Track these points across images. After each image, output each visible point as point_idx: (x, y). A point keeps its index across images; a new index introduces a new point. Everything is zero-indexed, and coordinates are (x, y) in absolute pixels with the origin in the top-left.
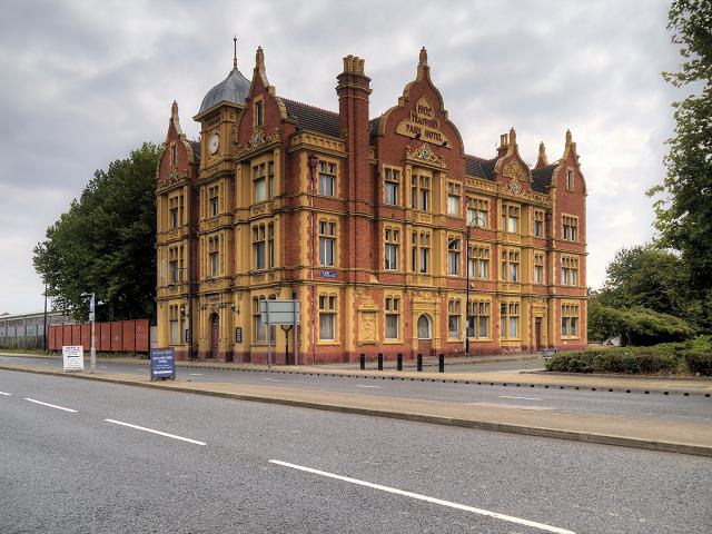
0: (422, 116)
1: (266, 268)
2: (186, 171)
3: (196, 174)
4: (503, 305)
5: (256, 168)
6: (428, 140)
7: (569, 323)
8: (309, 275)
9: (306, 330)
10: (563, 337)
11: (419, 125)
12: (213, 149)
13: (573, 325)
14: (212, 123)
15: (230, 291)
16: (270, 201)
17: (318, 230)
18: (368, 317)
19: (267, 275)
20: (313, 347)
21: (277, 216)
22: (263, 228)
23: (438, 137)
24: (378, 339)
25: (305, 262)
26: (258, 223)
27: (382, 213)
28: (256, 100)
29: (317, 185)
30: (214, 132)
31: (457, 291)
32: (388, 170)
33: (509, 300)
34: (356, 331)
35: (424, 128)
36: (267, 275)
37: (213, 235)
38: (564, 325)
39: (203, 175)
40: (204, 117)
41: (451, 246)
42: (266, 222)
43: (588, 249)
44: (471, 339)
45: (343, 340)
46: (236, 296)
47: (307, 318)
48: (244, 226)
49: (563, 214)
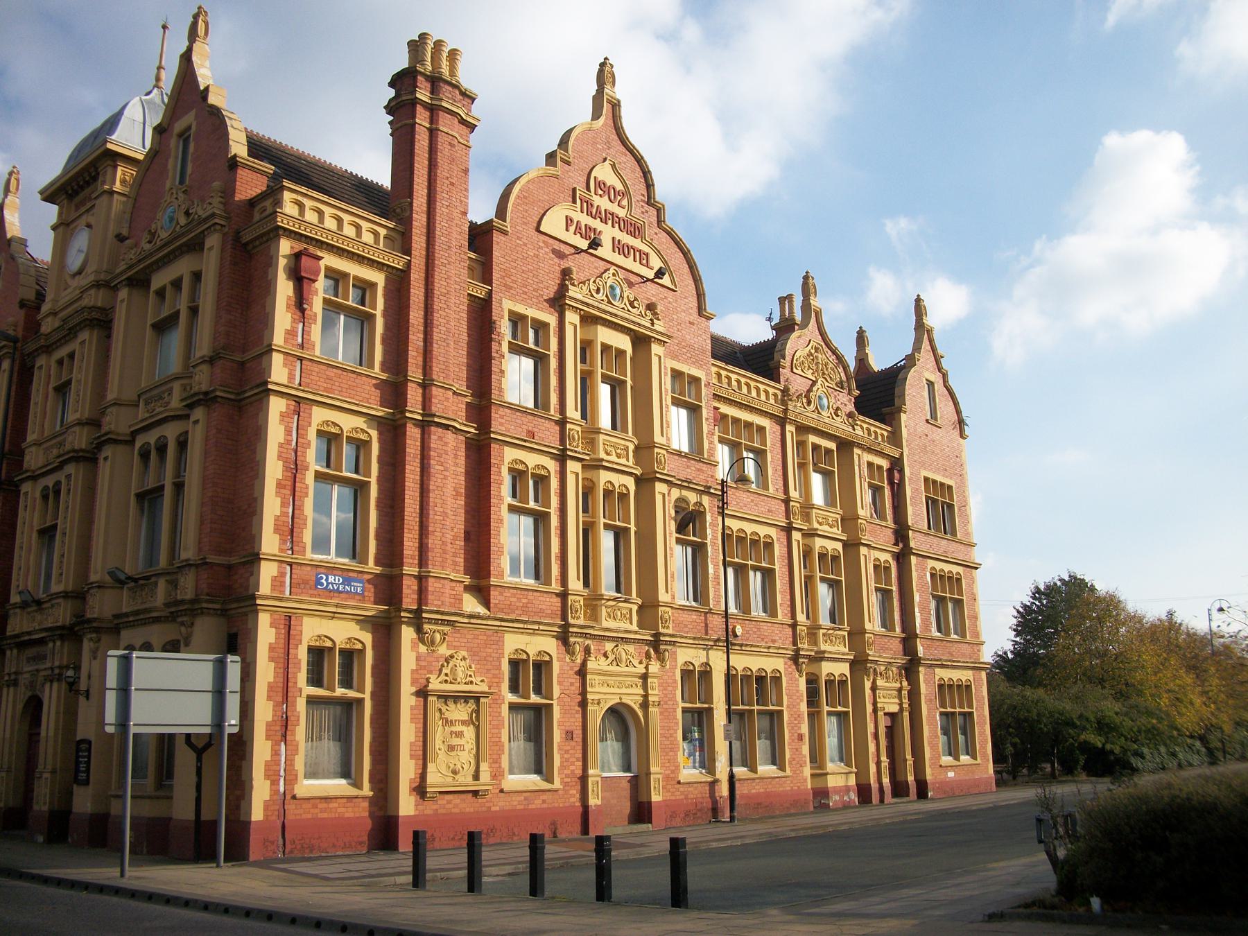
0: (603, 203)
4: (812, 681)
5: (161, 293)
6: (618, 259)
8: (277, 582)
9: (261, 750)
11: (596, 224)
16: (186, 375)
17: (302, 677)
18: (459, 712)
19: (162, 583)
20: (283, 800)
21: (199, 413)
22: (162, 449)
23: (643, 258)
25: (270, 542)
26: (151, 438)
27: (500, 423)
28: (179, 126)
30: (83, 221)
33: (827, 668)
35: (608, 233)
36: (162, 583)
39: (48, 326)
44: (740, 771)
48: (120, 449)
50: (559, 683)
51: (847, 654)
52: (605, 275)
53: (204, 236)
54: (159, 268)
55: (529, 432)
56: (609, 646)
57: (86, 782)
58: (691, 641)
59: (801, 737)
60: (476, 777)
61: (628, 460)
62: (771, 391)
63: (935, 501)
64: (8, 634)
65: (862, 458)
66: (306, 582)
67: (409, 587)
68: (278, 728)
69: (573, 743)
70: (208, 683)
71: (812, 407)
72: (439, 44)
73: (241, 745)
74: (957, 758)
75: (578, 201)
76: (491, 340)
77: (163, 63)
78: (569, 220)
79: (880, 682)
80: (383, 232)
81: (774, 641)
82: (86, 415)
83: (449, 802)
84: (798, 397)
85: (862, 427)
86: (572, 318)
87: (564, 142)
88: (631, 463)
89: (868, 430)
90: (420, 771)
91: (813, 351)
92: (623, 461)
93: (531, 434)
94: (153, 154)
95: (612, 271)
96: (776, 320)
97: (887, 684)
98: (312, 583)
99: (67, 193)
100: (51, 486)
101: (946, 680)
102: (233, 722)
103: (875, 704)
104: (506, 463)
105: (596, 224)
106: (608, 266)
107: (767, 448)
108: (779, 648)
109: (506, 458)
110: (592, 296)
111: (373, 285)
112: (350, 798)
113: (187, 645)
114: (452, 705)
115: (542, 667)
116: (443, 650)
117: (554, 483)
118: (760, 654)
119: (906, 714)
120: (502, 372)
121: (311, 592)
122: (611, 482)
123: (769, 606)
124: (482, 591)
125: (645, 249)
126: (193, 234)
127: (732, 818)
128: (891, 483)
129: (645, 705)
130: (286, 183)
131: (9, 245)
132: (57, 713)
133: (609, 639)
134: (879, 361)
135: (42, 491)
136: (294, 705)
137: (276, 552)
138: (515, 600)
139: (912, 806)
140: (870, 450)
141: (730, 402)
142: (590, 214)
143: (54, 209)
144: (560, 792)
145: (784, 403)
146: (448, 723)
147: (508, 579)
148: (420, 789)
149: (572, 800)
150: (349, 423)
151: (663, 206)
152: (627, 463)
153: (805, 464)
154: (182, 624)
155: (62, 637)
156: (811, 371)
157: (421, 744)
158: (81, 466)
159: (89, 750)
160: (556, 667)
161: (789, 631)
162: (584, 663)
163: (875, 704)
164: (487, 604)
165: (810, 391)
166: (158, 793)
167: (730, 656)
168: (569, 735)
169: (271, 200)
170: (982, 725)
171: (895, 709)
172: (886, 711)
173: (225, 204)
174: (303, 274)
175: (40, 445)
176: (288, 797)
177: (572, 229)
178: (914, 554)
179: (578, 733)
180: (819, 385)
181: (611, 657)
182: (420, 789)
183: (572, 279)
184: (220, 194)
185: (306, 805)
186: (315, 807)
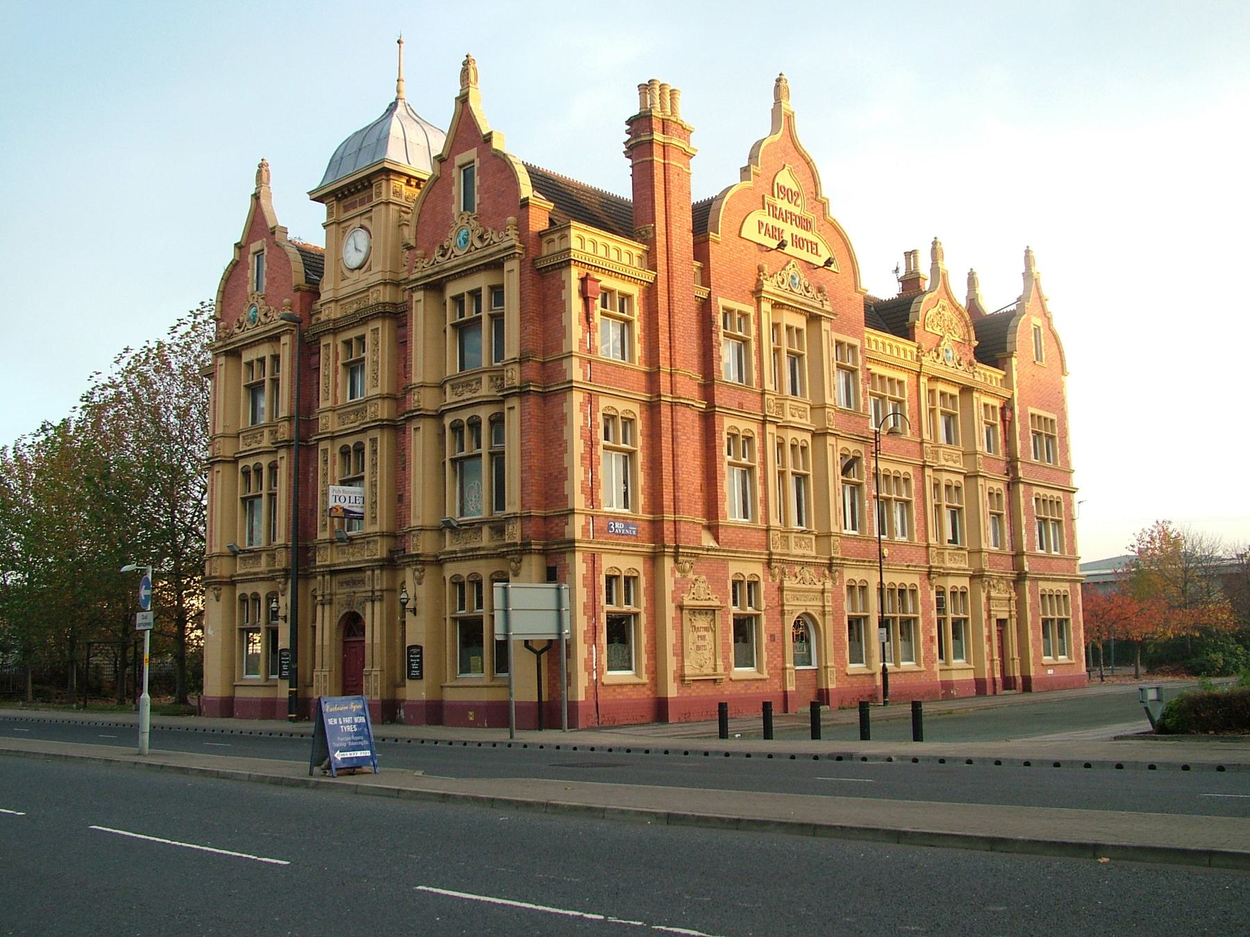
0: (783, 204)
1: (263, 544)
2: (289, 302)
3: (310, 312)
4: (940, 593)
7: (1053, 631)
8: (585, 530)
10: (1047, 659)
11: (779, 224)
12: (353, 258)
13: (956, 635)
14: (353, 206)
15: (392, 563)
18: (702, 622)
20: (596, 685)
22: (258, 470)
23: (813, 247)
24: (720, 670)
25: (579, 501)
26: (251, 463)
27: (720, 398)
29: (598, 337)
30: (357, 222)
31: (861, 562)
32: (728, 312)
33: (950, 583)
34: (681, 654)
37: (351, 442)
38: (1046, 635)
40: (333, 193)
41: (845, 471)
42: (265, 461)
43: (1076, 481)
45: (657, 672)
46: (409, 575)
47: (582, 623)
49: (1031, 410)
50: (765, 598)
51: (967, 570)
52: (788, 268)
53: (504, 260)
54: (455, 279)
55: (739, 403)
56: (797, 569)
57: (421, 677)
58: (854, 563)
59: (932, 639)
60: (715, 669)
61: (807, 420)
62: (908, 348)
63: (1039, 434)
64: (318, 563)
65: (979, 400)
66: (602, 529)
67: (668, 529)
68: (591, 635)
69: (775, 644)
70: (553, 606)
71: (940, 360)
72: (662, 87)
73: (570, 646)
74: (1056, 659)
75: (767, 206)
76: (711, 332)
77: (402, 76)
78: (760, 224)
79: (993, 594)
80: (636, 252)
81: (911, 561)
82: (386, 392)
83: (698, 687)
84: (929, 352)
85: (979, 373)
86: (766, 307)
87: (753, 157)
88: (809, 423)
89: (985, 375)
90: (679, 665)
91: (940, 310)
92: (803, 421)
93: (741, 405)
94: (435, 180)
95: (792, 263)
96: (902, 273)
97: (998, 595)
98: (606, 529)
99: (337, 196)
100: (351, 446)
101: (1054, 590)
102: (567, 631)
103: (989, 611)
104: (725, 430)
105: (779, 224)
106: (789, 258)
107: (906, 399)
108: (915, 566)
109: (726, 424)
110: (779, 287)
111: (629, 297)
112: (635, 685)
113: (516, 575)
114: (698, 617)
115: (753, 585)
116: (691, 576)
117: (757, 442)
118: (901, 571)
119: (1014, 620)
120: (720, 357)
121: (605, 535)
122: (795, 438)
123: (907, 529)
124: (713, 529)
125: (815, 240)
126: (494, 258)
127: (885, 703)
128: (1003, 420)
129: (824, 614)
130: (573, 223)
131: (273, 233)
132: (381, 625)
133: (797, 563)
134: (990, 305)
135: (341, 448)
136: (599, 619)
137: (583, 508)
138: (734, 535)
139: (1015, 697)
140: (986, 393)
141: (878, 362)
142: (775, 216)
143: (322, 208)
144: (768, 681)
145: (918, 359)
146: (696, 629)
147: (730, 519)
148: (681, 678)
149: (776, 687)
150: (621, 407)
151: (828, 200)
152: (805, 422)
153: (935, 409)
154: (513, 560)
155: (382, 567)
156: (939, 328)
157: (680, 645)
158: (386, 432)
159: (421, 653)
160: (762, 585)
161: (923, 551)
162: (782, 581)
163: (989, 611)
164: (716, 539)
165: (938, 345)
166: (493, 683)
167: (883, 574)
168: (772, 638)
169: (559, 234)
170: (1076, 629)
171: (1005, 616)
172: (998, 617)
173: (519, 236)
174: (589, 295)
175: (334, 411)
176: (599, 684)
177: (763, 231)
178: (1022, 482)
179: (778, 636)
180: (945, 340)
181: (799, 577)
182: (681, 678)
183: (764, 274)
184: (515, 227)
185: (611, 690)
186: (614, 691)
